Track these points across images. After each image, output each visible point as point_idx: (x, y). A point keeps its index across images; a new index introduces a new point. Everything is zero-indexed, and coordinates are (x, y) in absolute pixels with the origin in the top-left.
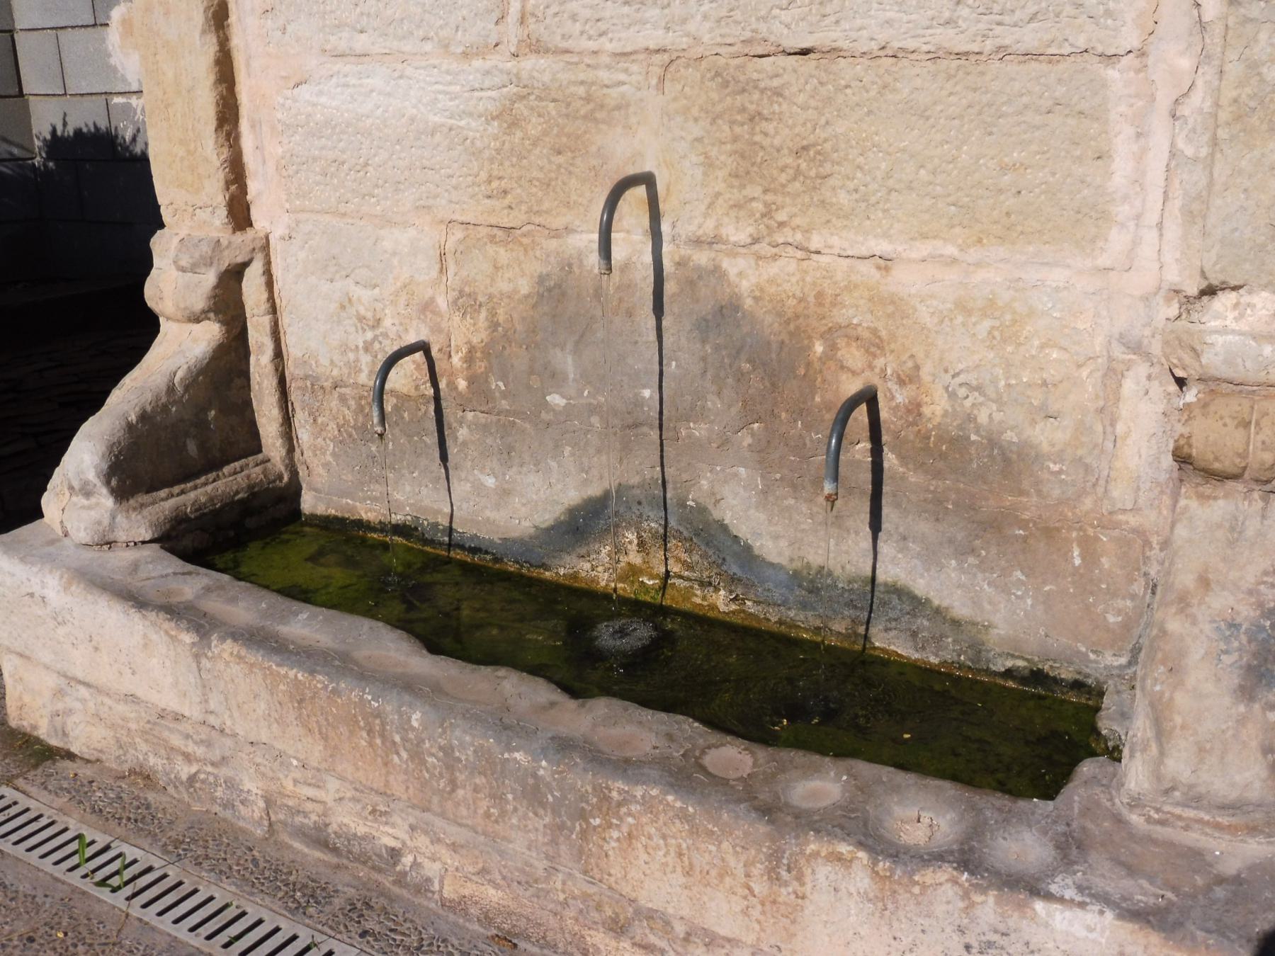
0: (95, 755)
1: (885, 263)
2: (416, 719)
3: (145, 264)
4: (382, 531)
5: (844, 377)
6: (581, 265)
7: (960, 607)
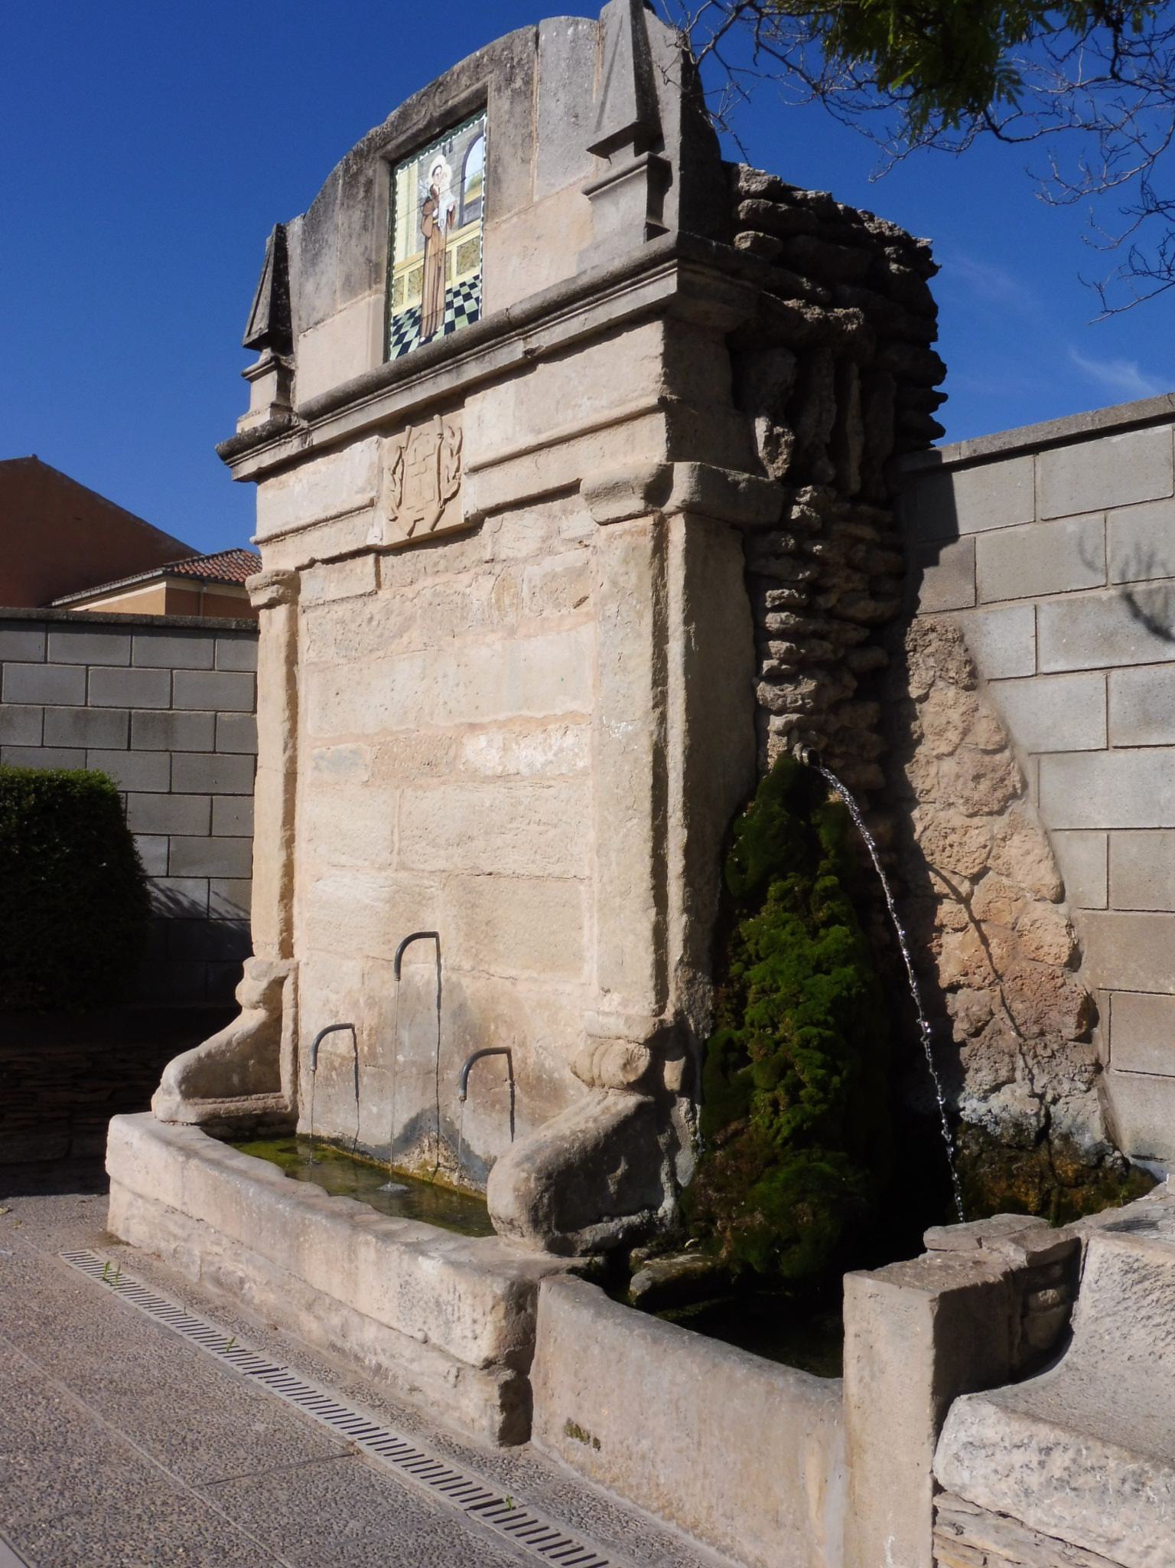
3: (239, 975)
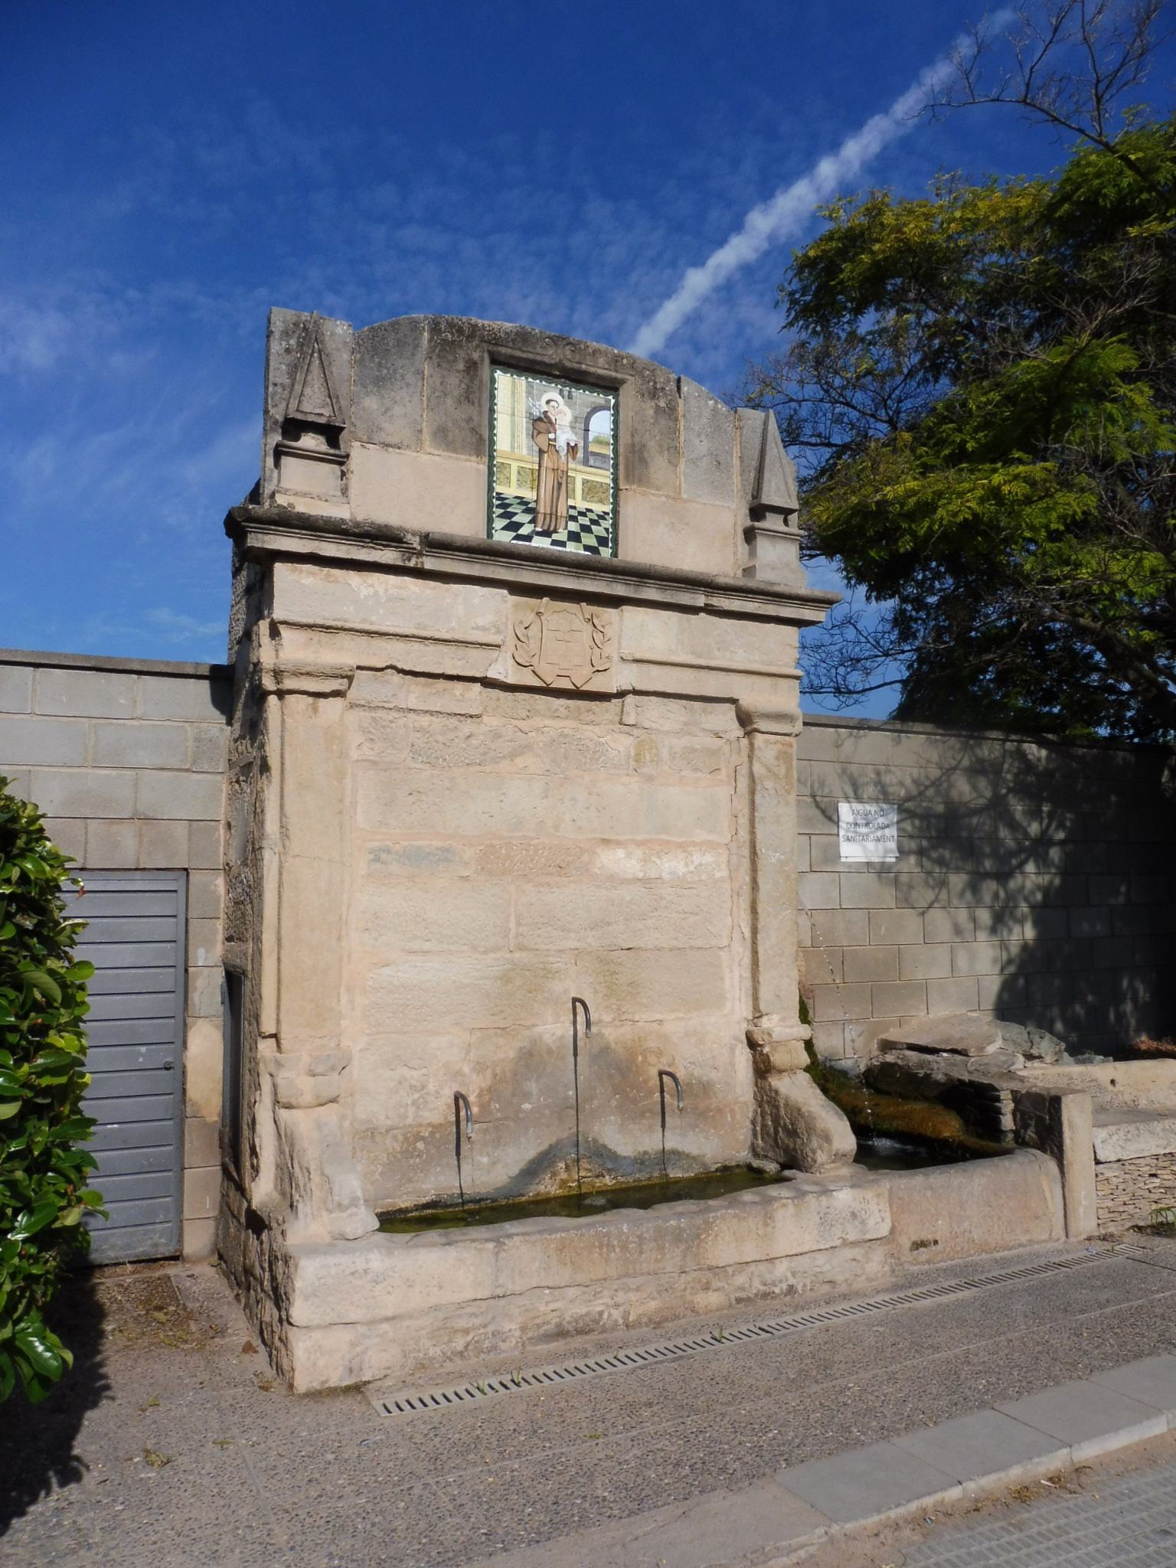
0: (384, 1372)
1: (661, 1022)
2: (625, 1228)
4: (417, 1210)
5: (650, 1068)
6: (541, 1040)
7: (695, 1152)
